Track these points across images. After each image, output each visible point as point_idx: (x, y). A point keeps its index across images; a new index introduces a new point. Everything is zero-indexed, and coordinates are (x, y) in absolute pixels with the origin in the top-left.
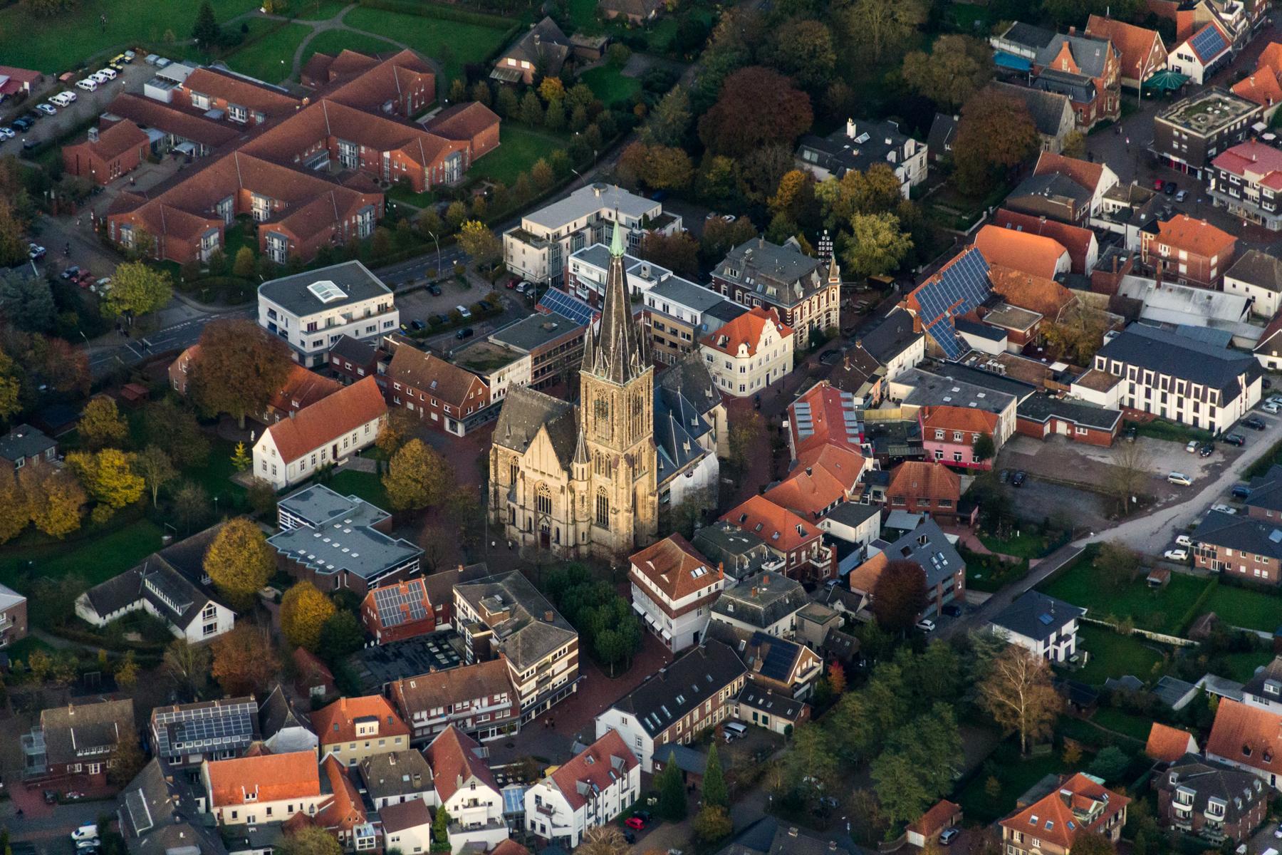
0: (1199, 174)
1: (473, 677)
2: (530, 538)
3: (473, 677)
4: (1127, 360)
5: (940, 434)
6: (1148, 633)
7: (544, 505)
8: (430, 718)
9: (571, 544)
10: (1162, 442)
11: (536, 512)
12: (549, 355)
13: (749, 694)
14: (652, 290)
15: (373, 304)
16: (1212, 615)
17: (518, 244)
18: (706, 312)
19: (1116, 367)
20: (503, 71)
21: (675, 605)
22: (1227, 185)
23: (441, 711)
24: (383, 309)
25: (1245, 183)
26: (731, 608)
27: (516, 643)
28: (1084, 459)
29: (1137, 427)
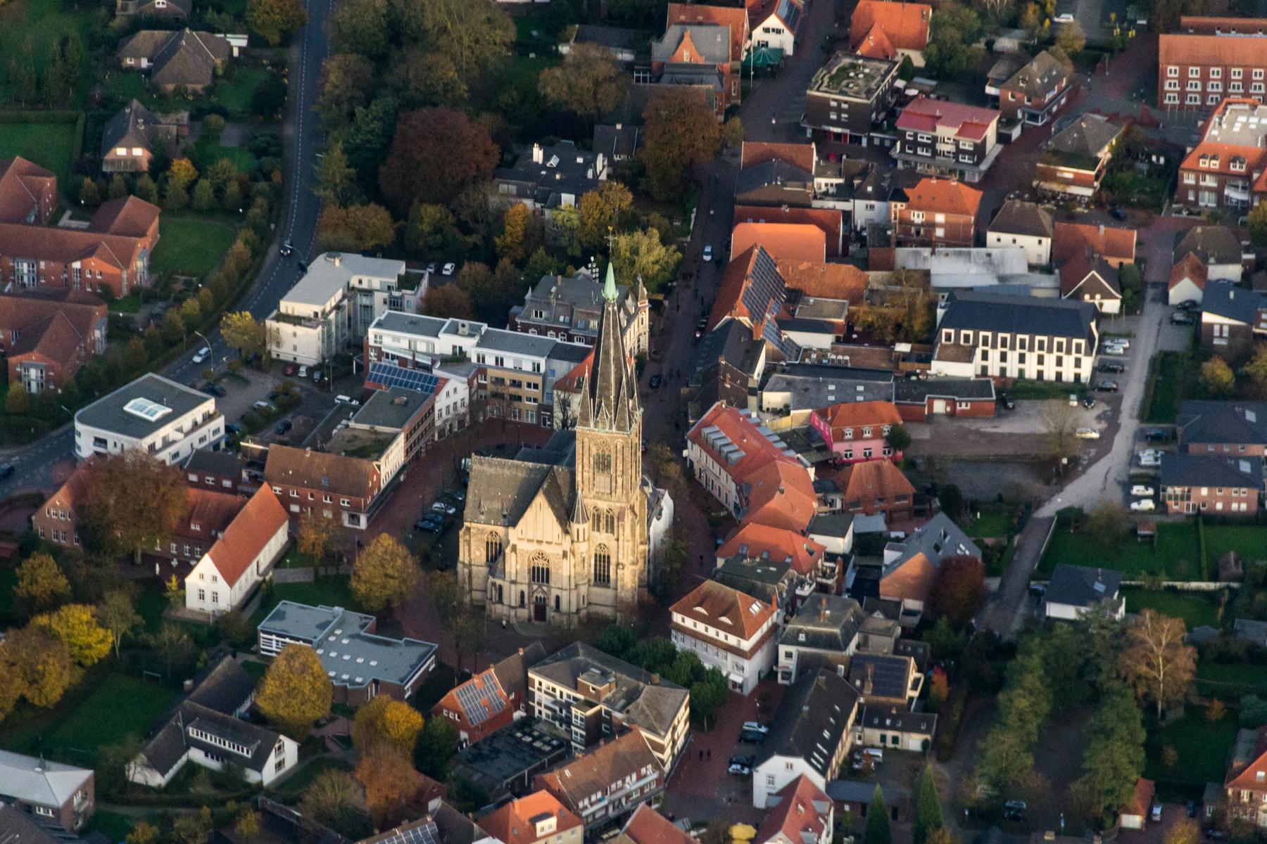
0: (864, 142)
1: (616, 755)
2: (524, 613)
3: (616, 755)
4: (977, 327)
5: (849, 432)
6: (1179, 584)
7: (540, 575)
8: (592, 804)
9: (574, 609)
10: (1039, 403)
11: (529, 585)
12: (415, 430)
13: (869, 717)
14: (478, 345)
15: (197, 413)
16: (1232, 555)
17: (286, 329)
18: (549, 357)
19: (967, 338)
20: (113, 162)
21: (746, 645)
22: (915, 144)
23: (599, 795)
24: (208, 418)
25: (935, 139)
26: (802, 637)
27: (643, 712)
28: (977, 432)
29: (1012, 393)
